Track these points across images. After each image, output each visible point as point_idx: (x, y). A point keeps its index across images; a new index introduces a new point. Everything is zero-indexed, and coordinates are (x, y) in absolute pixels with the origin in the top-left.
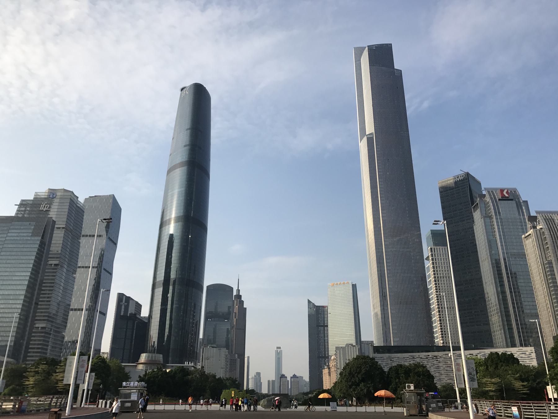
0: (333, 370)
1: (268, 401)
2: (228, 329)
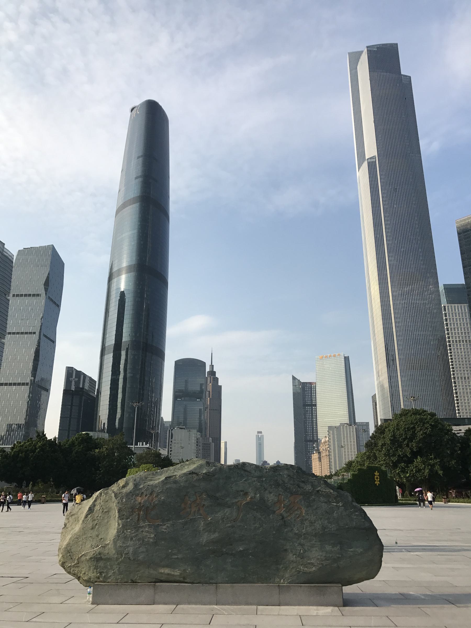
0: (323, 454)
1: (134, 513)
2: (200, 410)
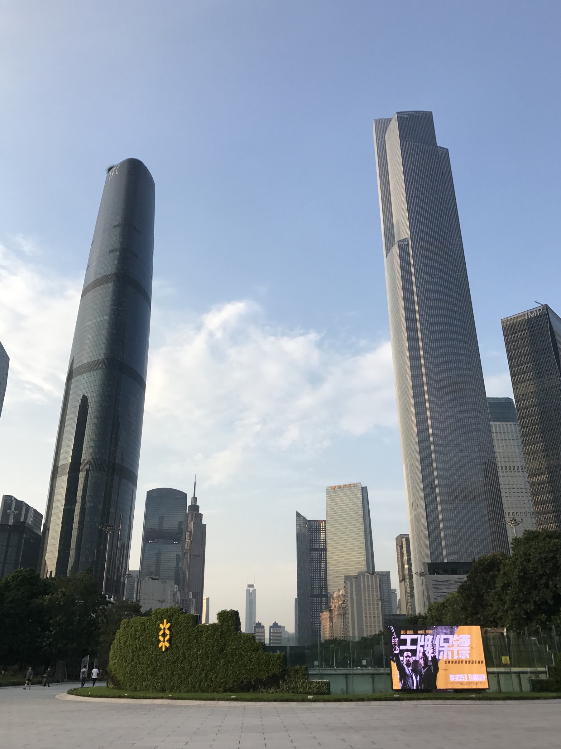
0: (335, 613)
